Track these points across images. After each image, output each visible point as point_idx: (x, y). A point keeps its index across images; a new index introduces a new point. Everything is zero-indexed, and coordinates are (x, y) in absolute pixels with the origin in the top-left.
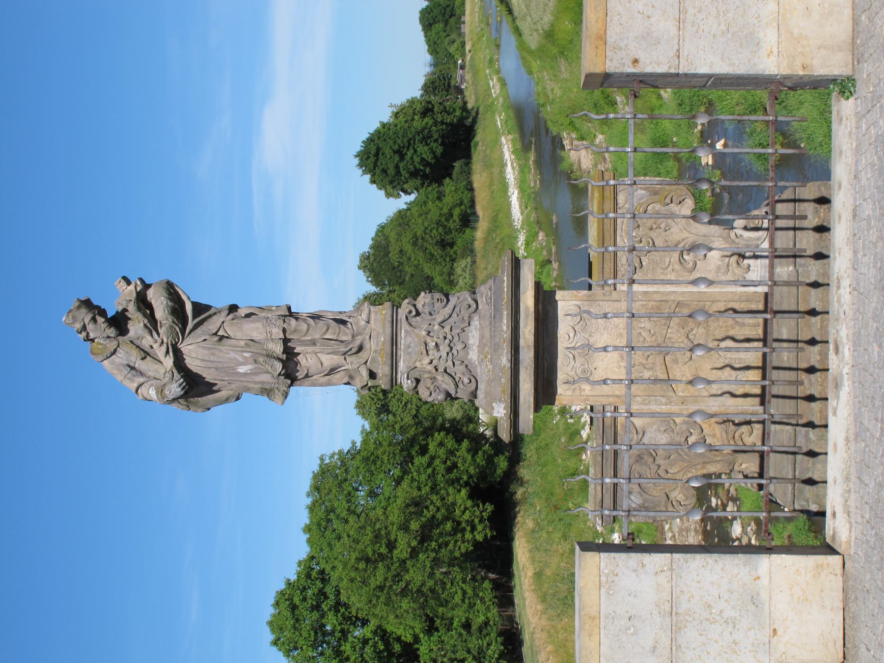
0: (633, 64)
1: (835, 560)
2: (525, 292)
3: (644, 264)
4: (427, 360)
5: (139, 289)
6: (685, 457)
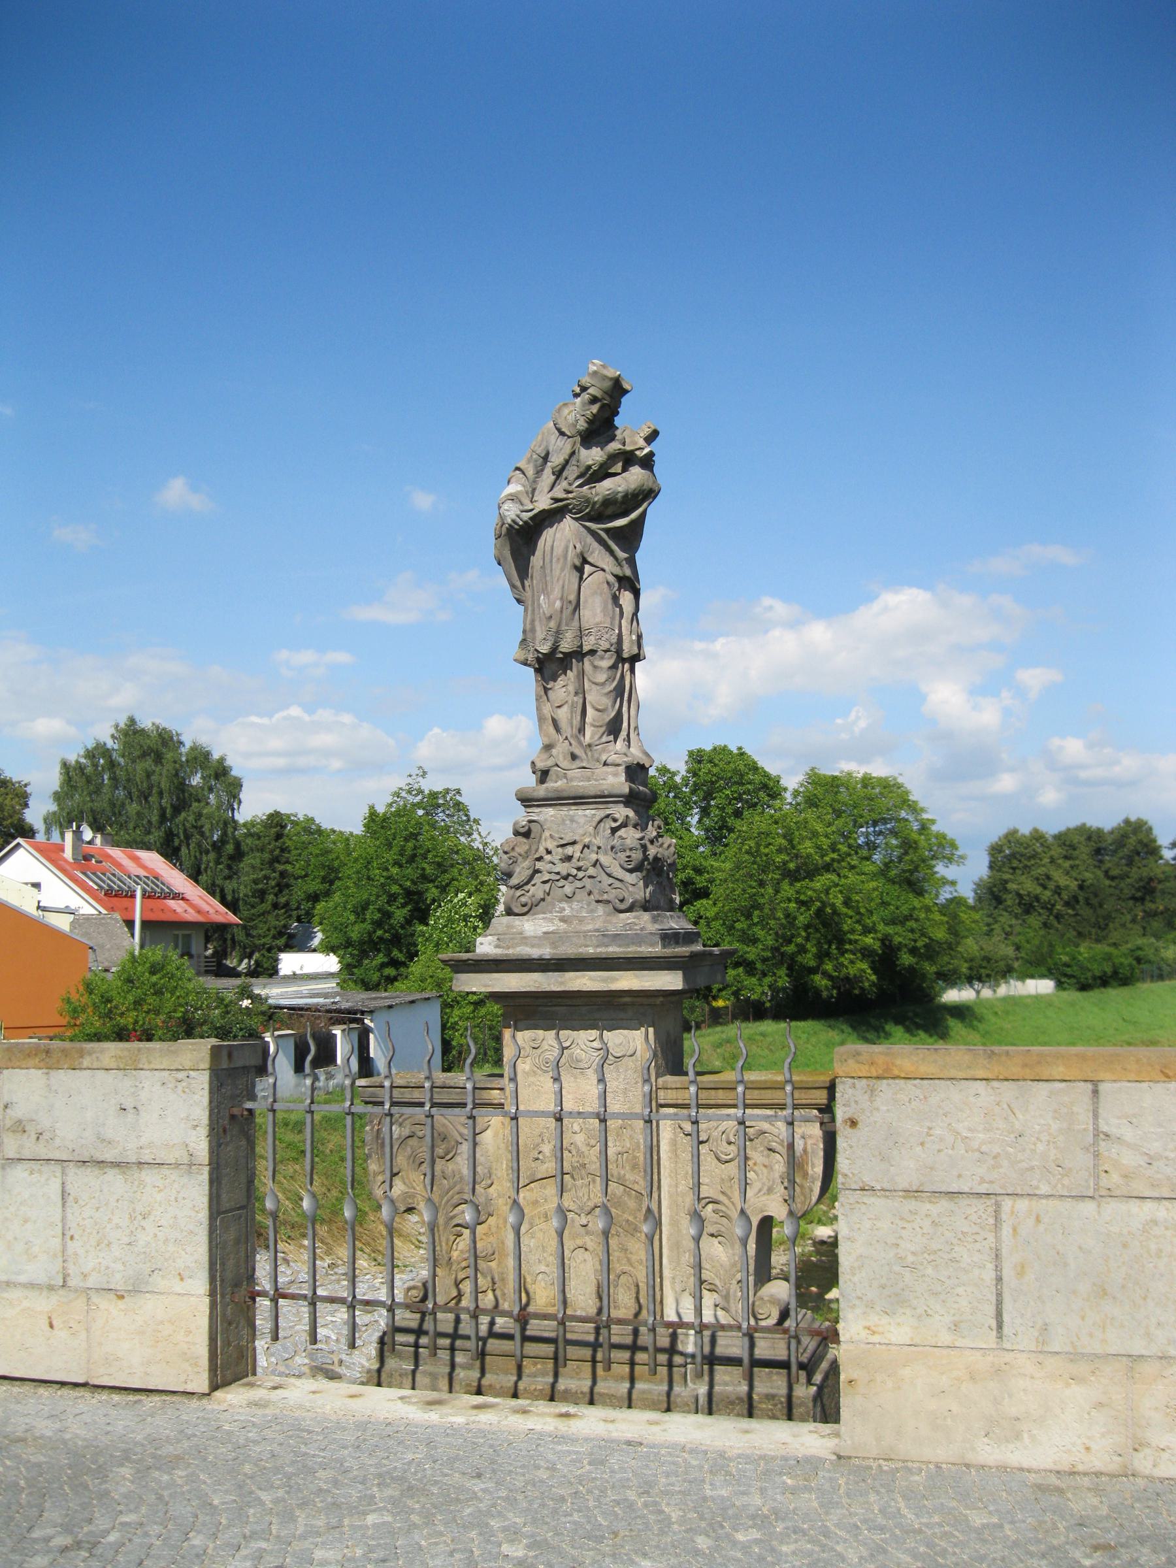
0: (849, 1119)
1: (201, 1383)
2: (637, 977)
4: (551, 845)
5: (637, 453)
6: (446, 1198)
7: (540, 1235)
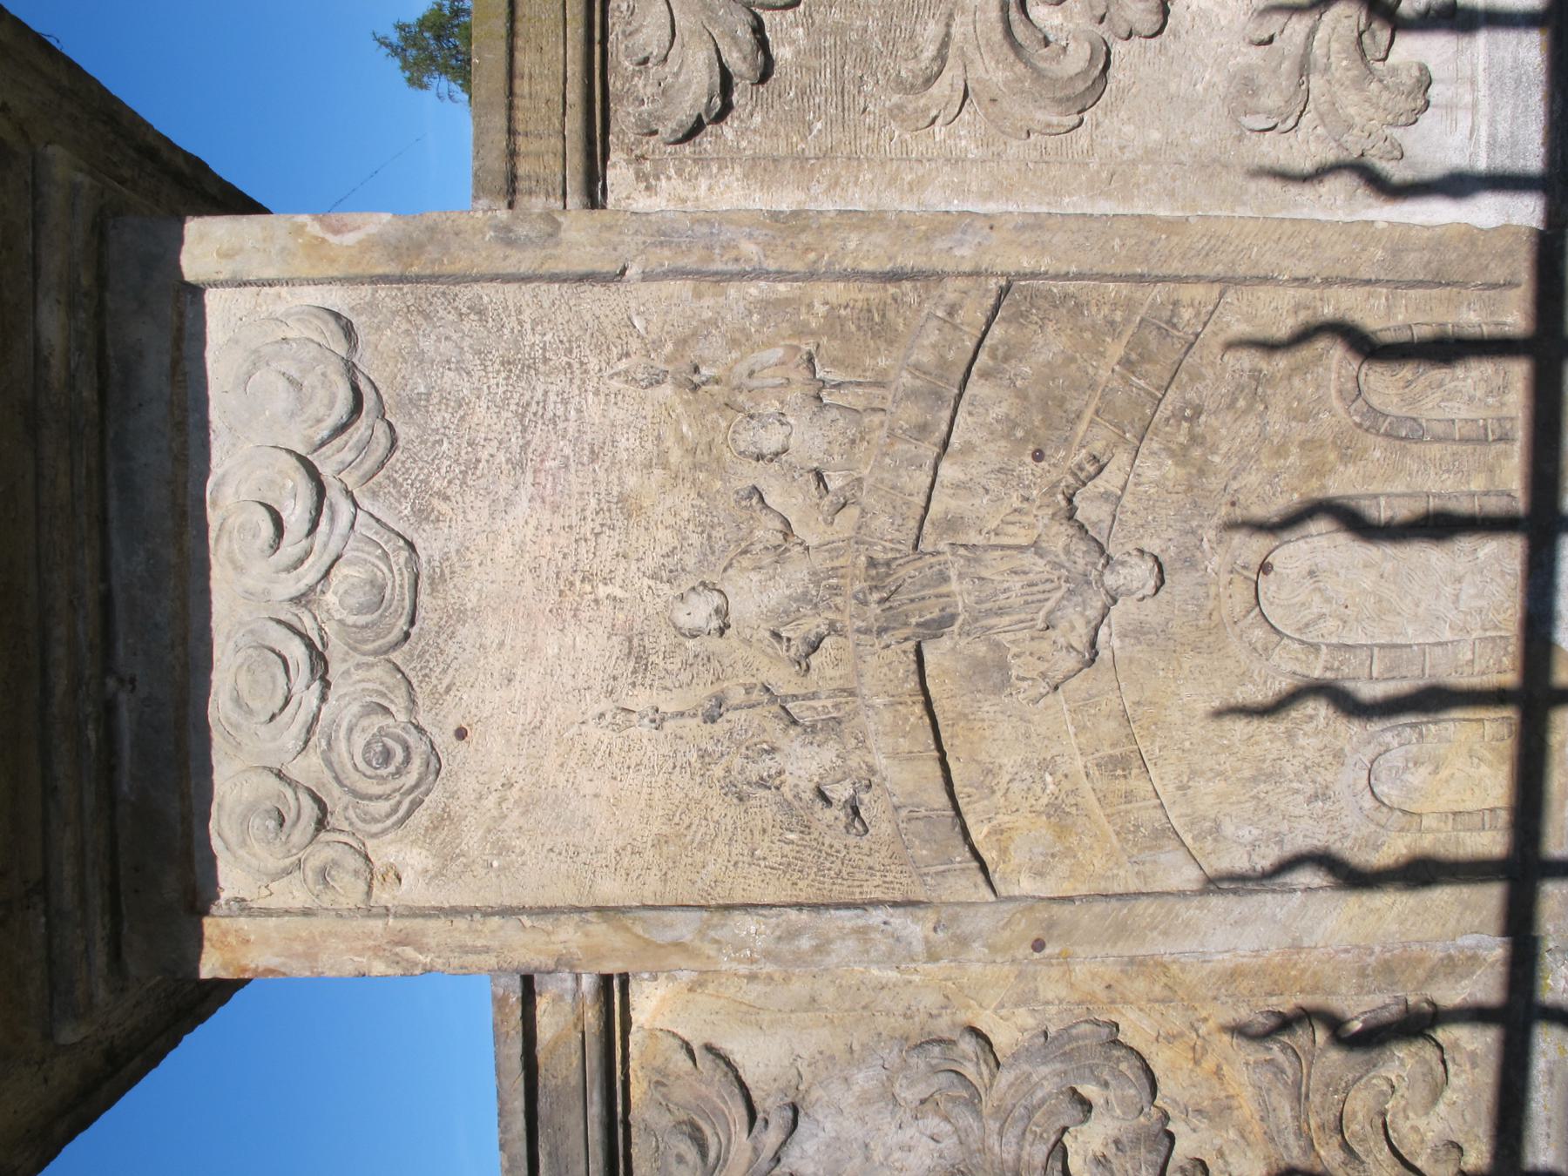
3: (782, 53)
7: (1207, 793)
